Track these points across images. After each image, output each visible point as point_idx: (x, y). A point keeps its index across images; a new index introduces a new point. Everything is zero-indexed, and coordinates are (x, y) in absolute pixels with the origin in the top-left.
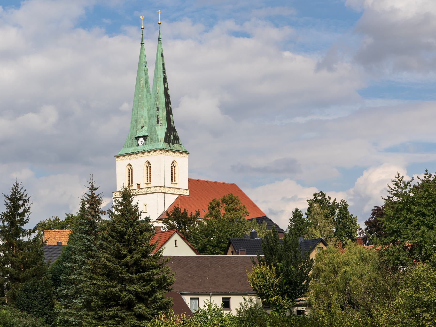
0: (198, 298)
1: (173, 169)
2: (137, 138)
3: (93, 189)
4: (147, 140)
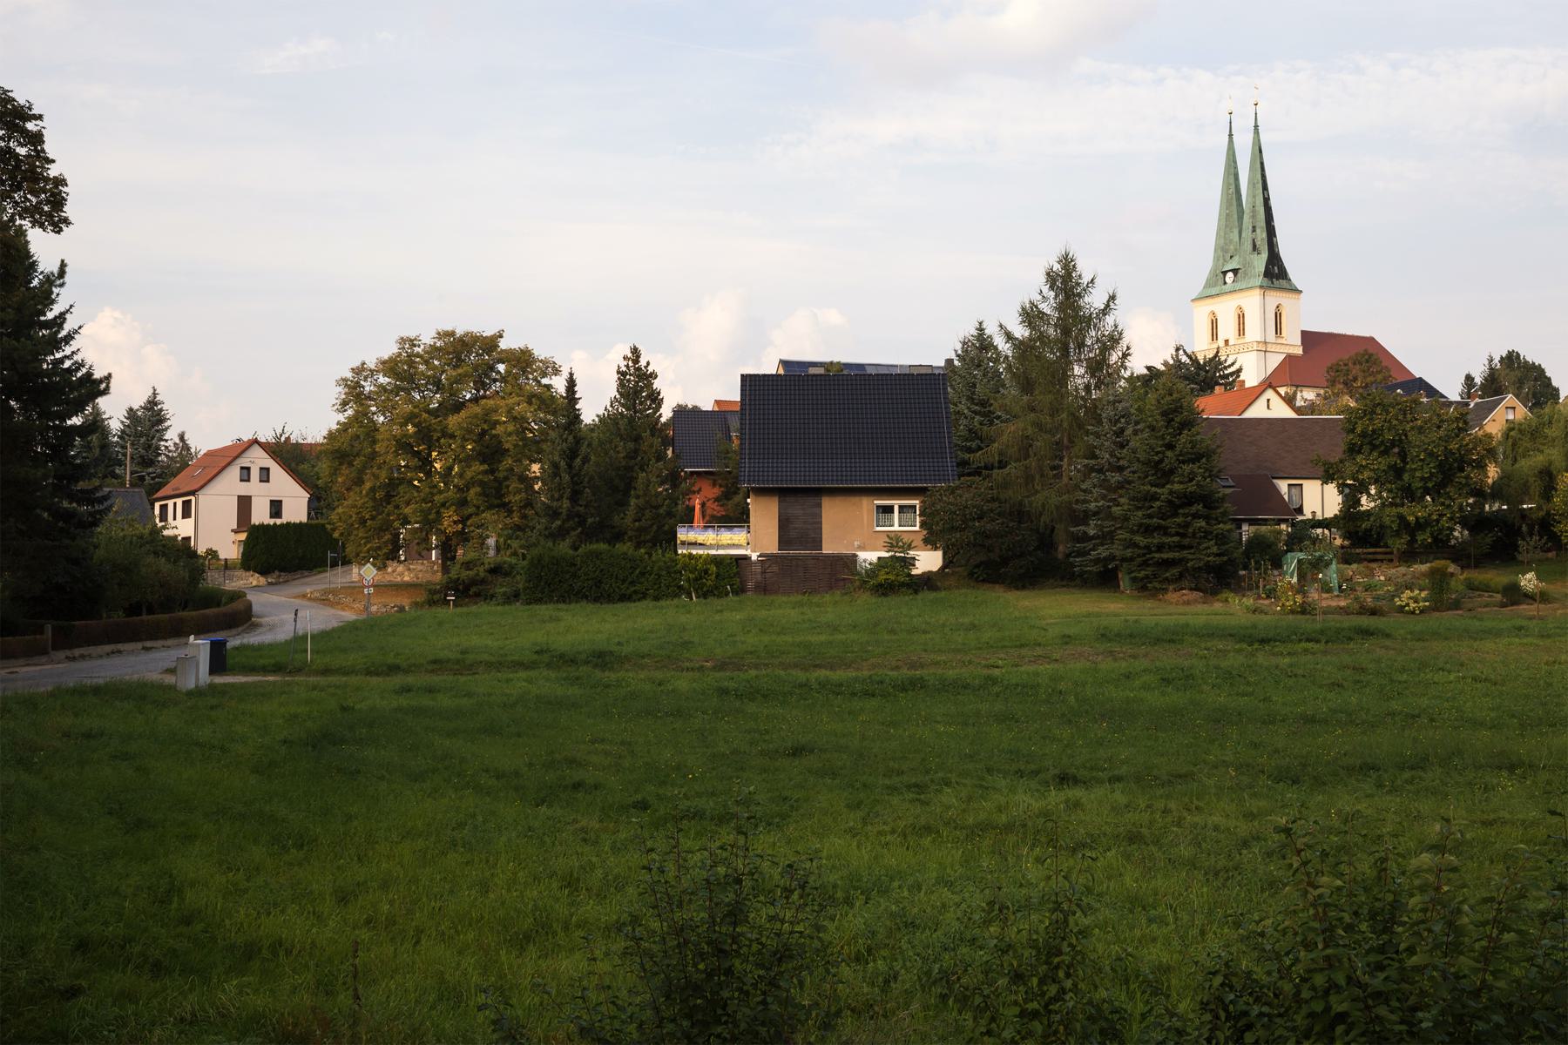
0: (1301, 485)
1: (1278, 317)
2: (1225, 273)
3: (155, 394)
4: (1239, 275)
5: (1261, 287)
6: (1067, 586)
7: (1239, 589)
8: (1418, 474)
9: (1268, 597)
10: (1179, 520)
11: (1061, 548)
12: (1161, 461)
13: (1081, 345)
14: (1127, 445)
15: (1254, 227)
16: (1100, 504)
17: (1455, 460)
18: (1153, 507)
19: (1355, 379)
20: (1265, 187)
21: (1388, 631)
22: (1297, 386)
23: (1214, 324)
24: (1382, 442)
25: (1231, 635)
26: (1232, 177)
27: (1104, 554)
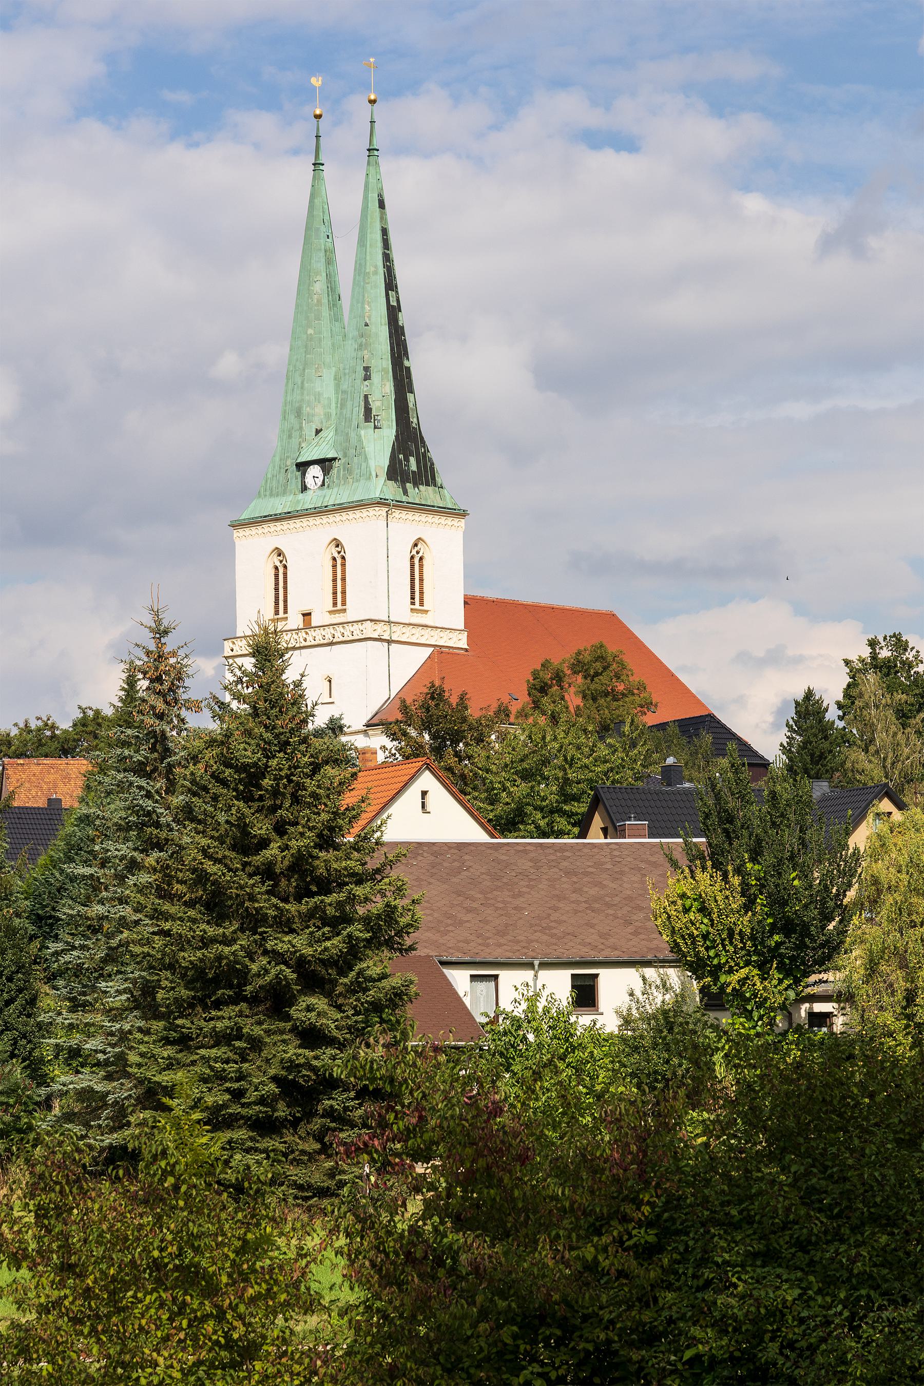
0: (496, 977)
2: (303, 467)
4: (334, 472)
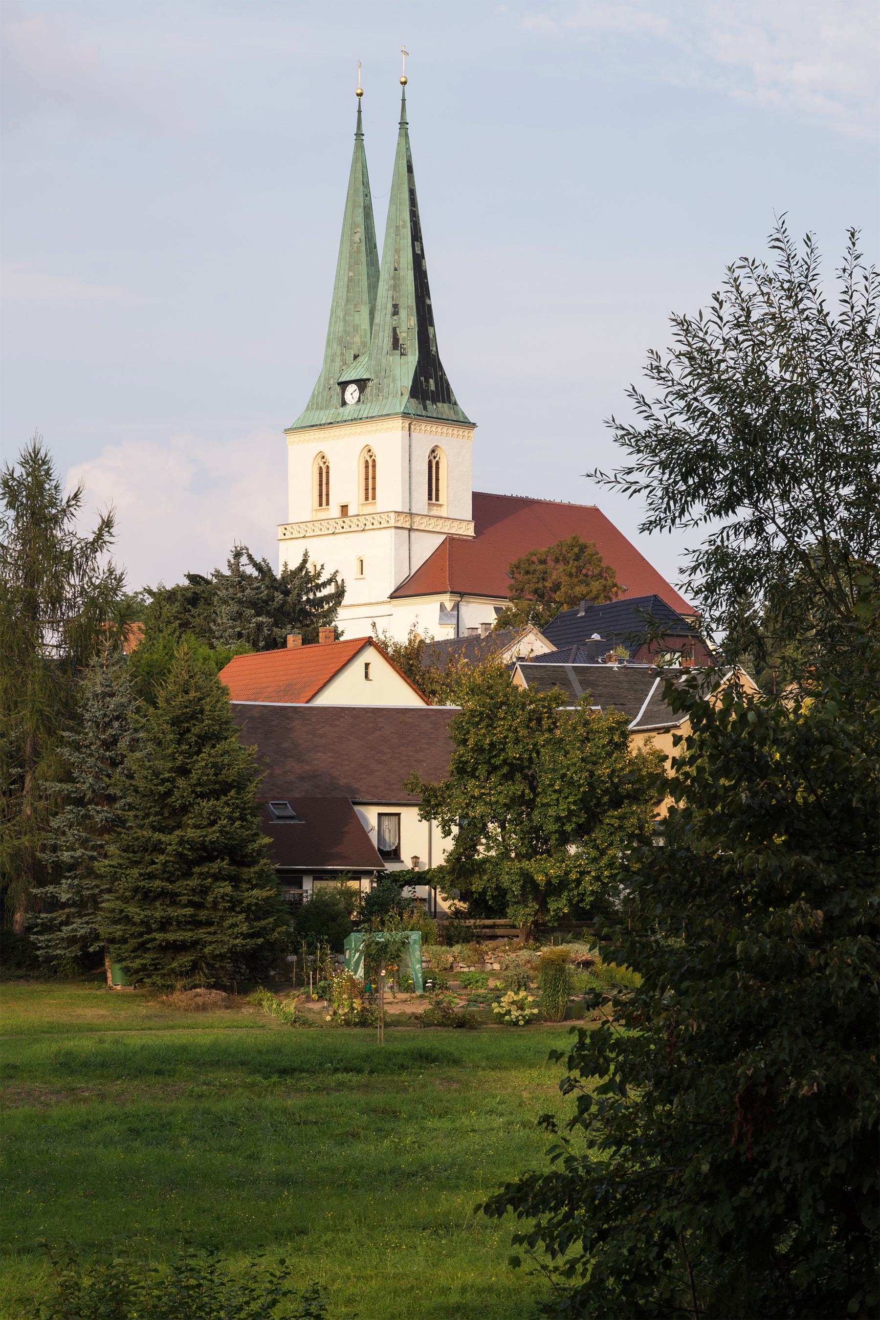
0: (399, 815)
1: (433, 468)
2: (344, 385)
4: (368, 390)
5: (405, 415)
6: (26, 978)
7: (276, 987)
8: (551, 812)
9: (321, 998)
10: (193, 883)
11: (18, 917)
12: (169, 793)
13: (56, 599)
14: (122, 763)
15: (395, 306)
16: (78, 853)
17: (606, 792)
18: (154, 863)
19: (556, 587)
20: (416, 236)
21: (457, 1055)
22: (462, 595)
23: (323, 476)
24: (505, 761)
25: (243, 1063)
26: (360, 211)
27: (83, 931)
